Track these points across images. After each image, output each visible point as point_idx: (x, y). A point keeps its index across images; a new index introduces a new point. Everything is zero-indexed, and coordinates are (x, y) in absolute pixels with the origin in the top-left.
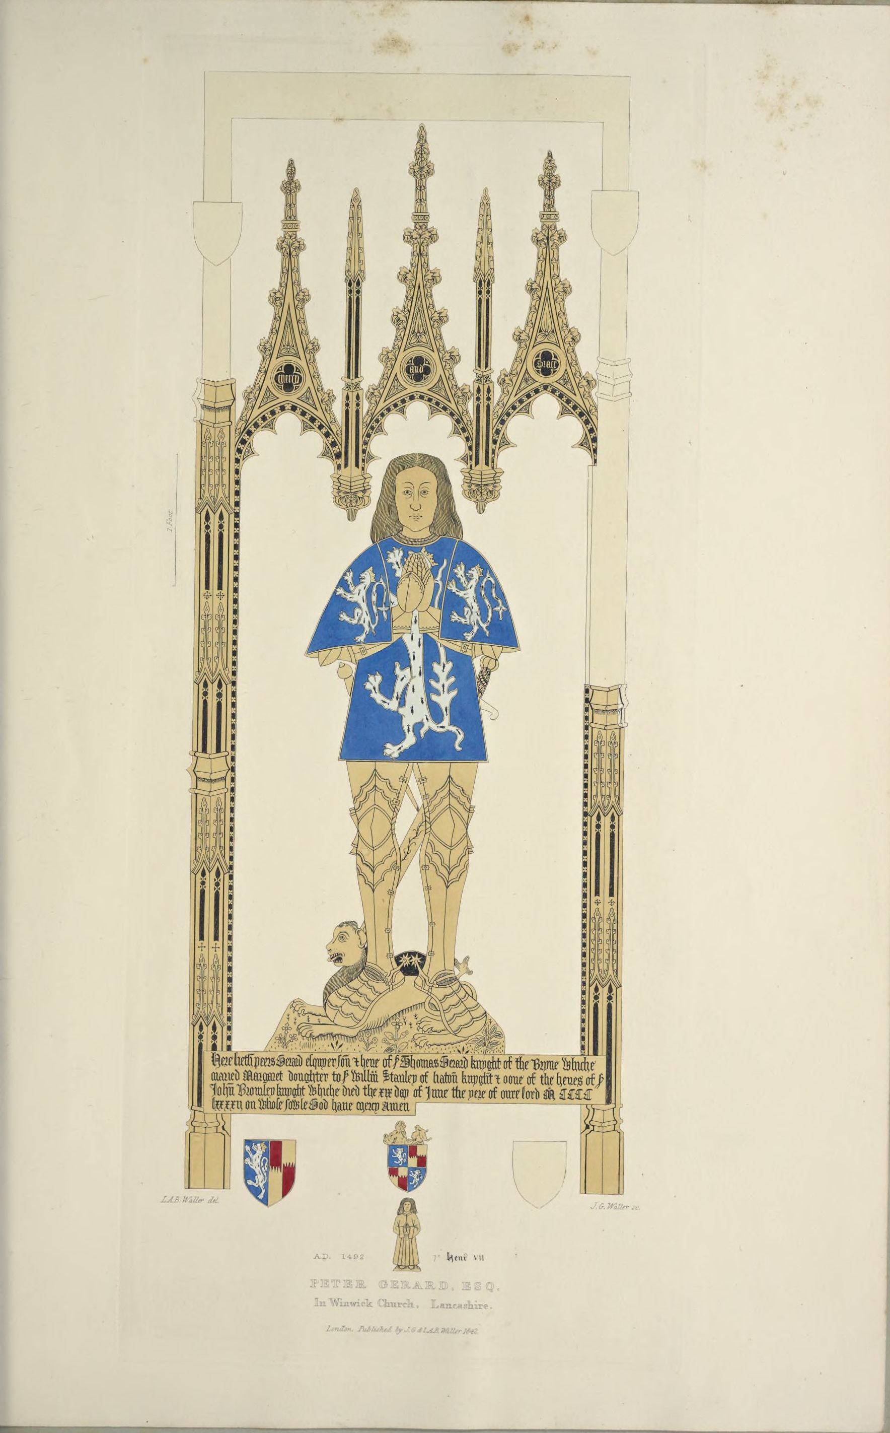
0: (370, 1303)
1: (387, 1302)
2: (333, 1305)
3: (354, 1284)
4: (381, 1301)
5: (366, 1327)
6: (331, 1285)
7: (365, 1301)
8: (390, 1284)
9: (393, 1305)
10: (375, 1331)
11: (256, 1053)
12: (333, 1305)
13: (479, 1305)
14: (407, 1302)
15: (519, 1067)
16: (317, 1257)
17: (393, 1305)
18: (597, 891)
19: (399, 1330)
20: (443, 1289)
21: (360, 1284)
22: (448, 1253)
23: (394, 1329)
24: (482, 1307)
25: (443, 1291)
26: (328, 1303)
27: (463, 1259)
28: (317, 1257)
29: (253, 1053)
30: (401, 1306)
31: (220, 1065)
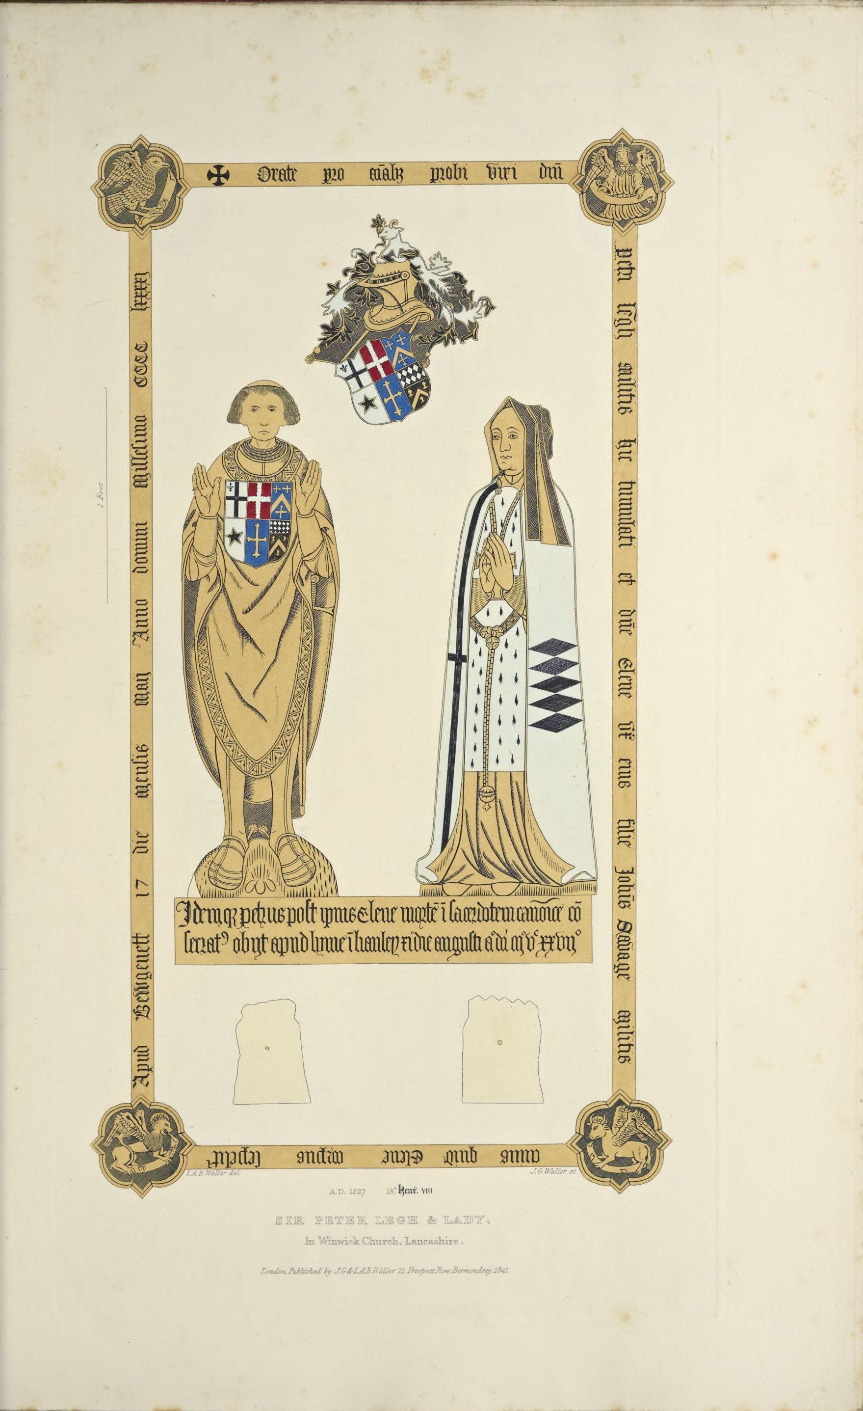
0: (357, 1241)
1: (373, 1239)
2: (322, 1243)
3: (356, 1220)
4: (366, 1239)
5: (296, 1269)
6: (383, 1219)
7: (352, 1239)
8: (406, 1219)
9: (379, 1242)
10: (303, 1273)
11: (634, 903)
12: (322, 1243)
13: (450, 1240)
14: (391, 1239)
15: (572, 917)
16: (332, 1192)
17: (379, 1242)
18: (468, 552)
19: (328, 1272)
20: (468, 1223)
21: (414, 1220)
22: (399, 1186)
23: (323, 1270)
24: (452, 1243)
25: (469, 1225)
26: (317, 1241)
27: (412, 1191)
28: (332, 1192)
29: (635, 900)
30: (386, 1243)
31: (260, 953)
